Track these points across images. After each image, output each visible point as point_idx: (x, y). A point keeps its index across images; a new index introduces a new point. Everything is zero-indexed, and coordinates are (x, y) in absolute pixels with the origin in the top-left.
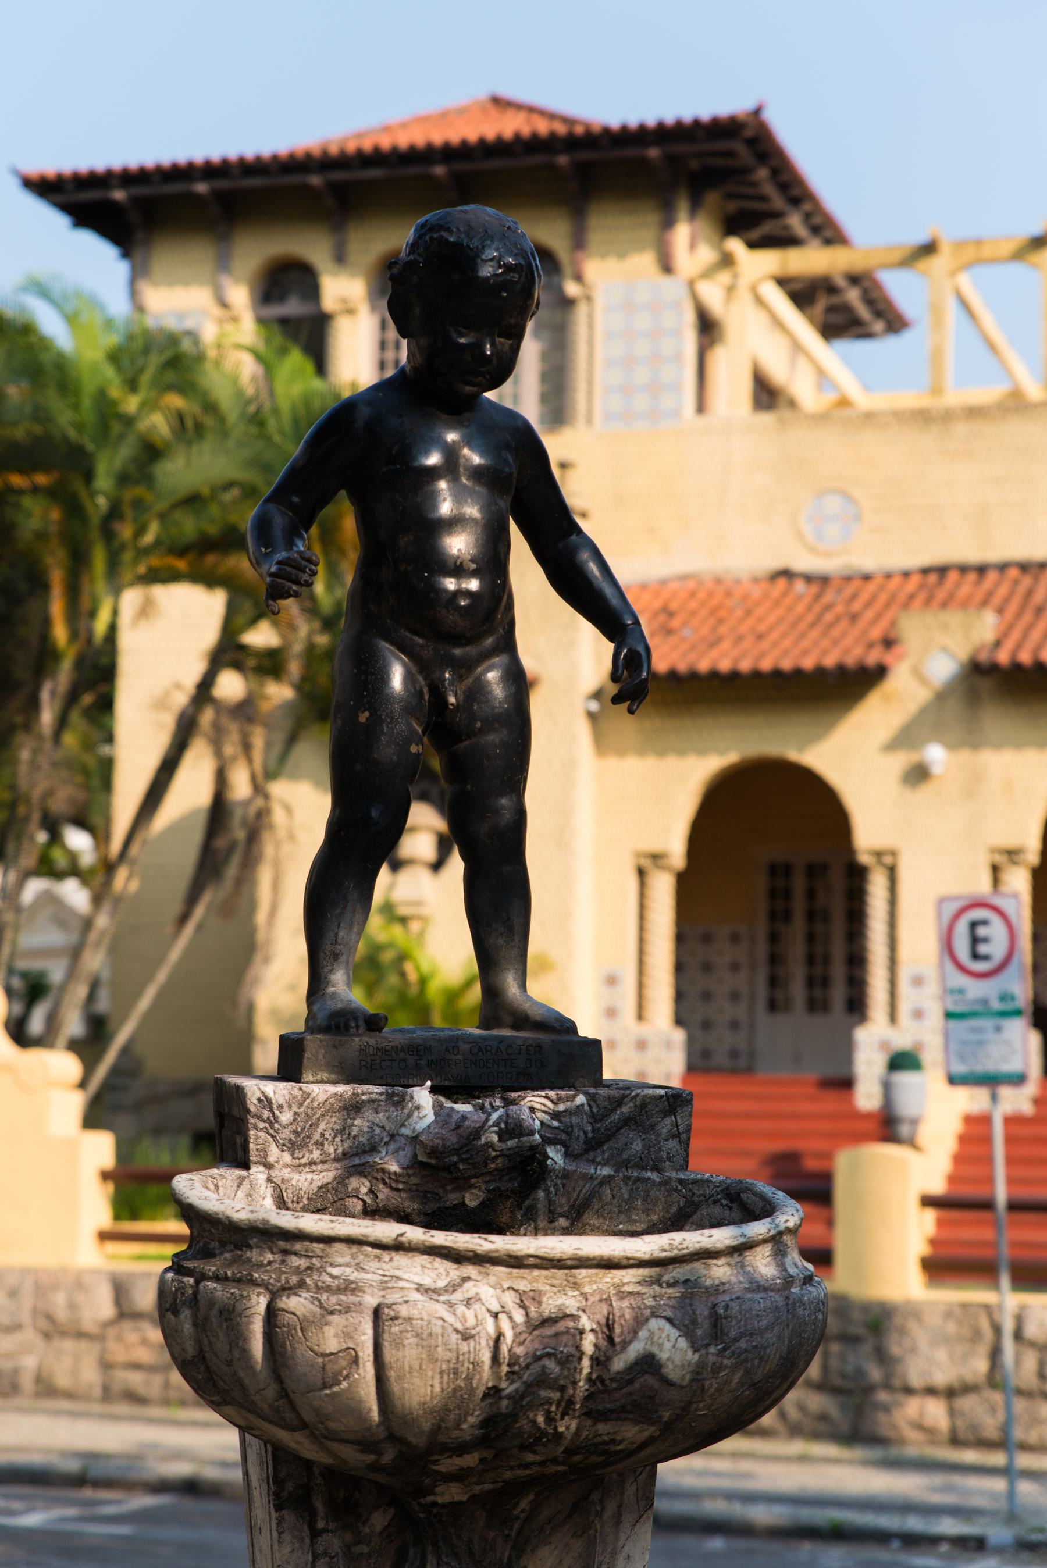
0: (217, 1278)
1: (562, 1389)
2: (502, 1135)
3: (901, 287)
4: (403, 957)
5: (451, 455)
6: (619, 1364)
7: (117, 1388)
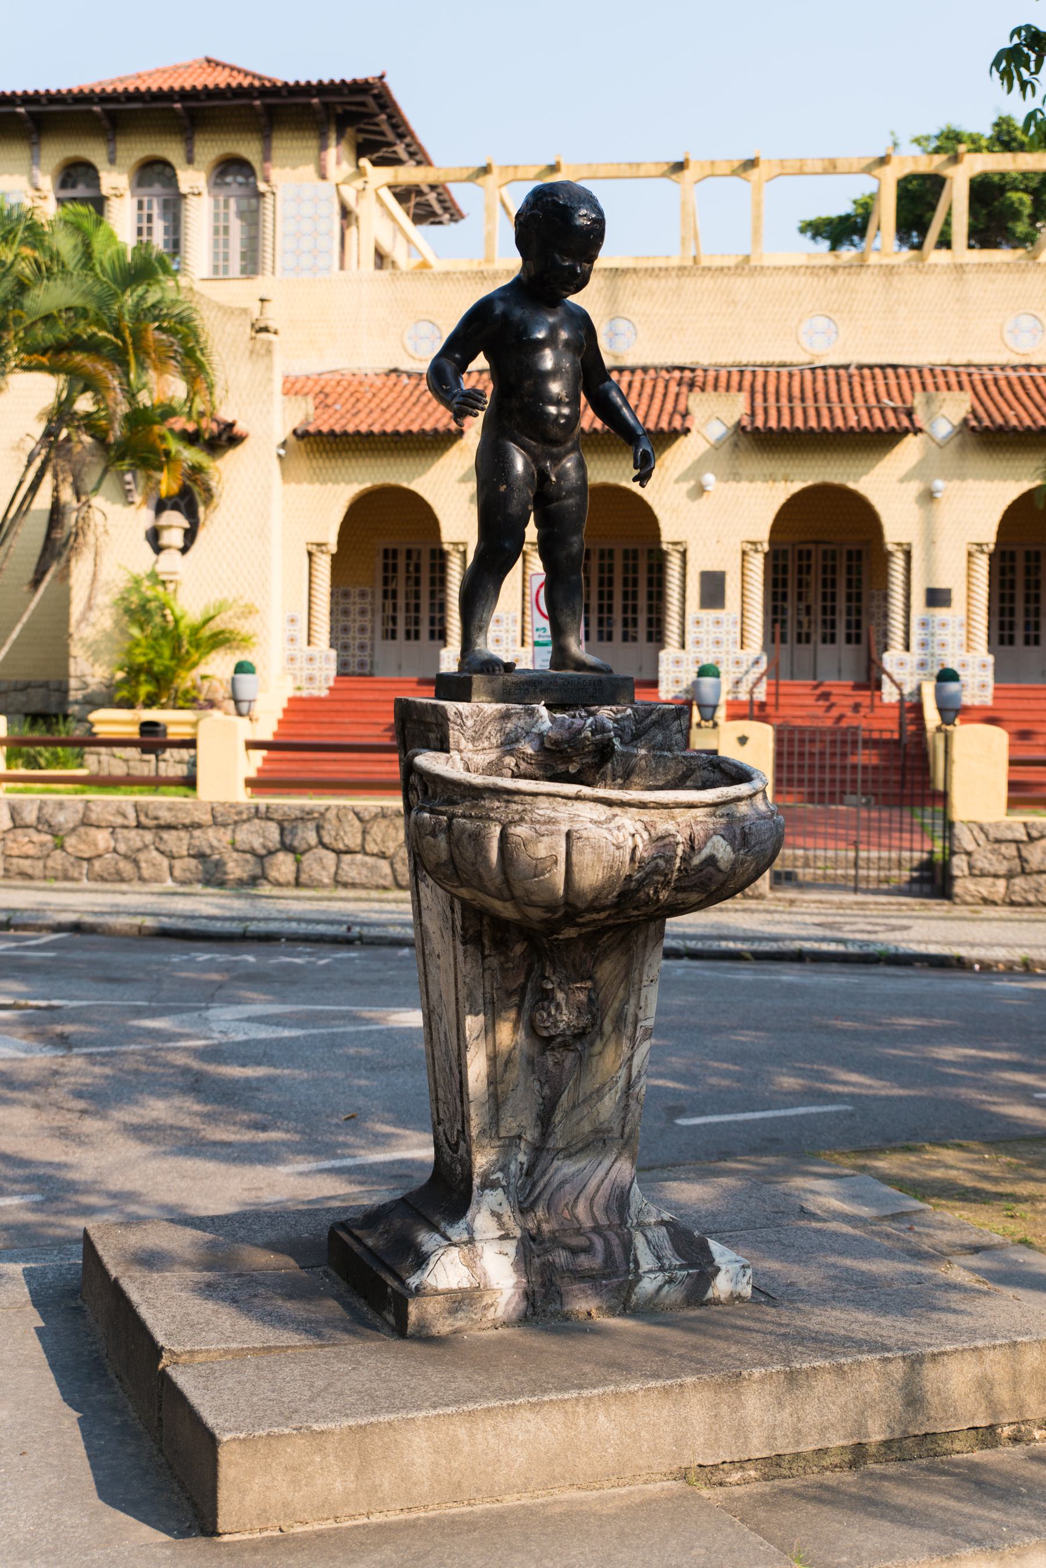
0: (464, 816)
1: (666, 875)
2: (593, 733)
3: (461, 194)
4: (163, 607)
5: (553, 331)
6: (696, 861)
7: (14, 869)
